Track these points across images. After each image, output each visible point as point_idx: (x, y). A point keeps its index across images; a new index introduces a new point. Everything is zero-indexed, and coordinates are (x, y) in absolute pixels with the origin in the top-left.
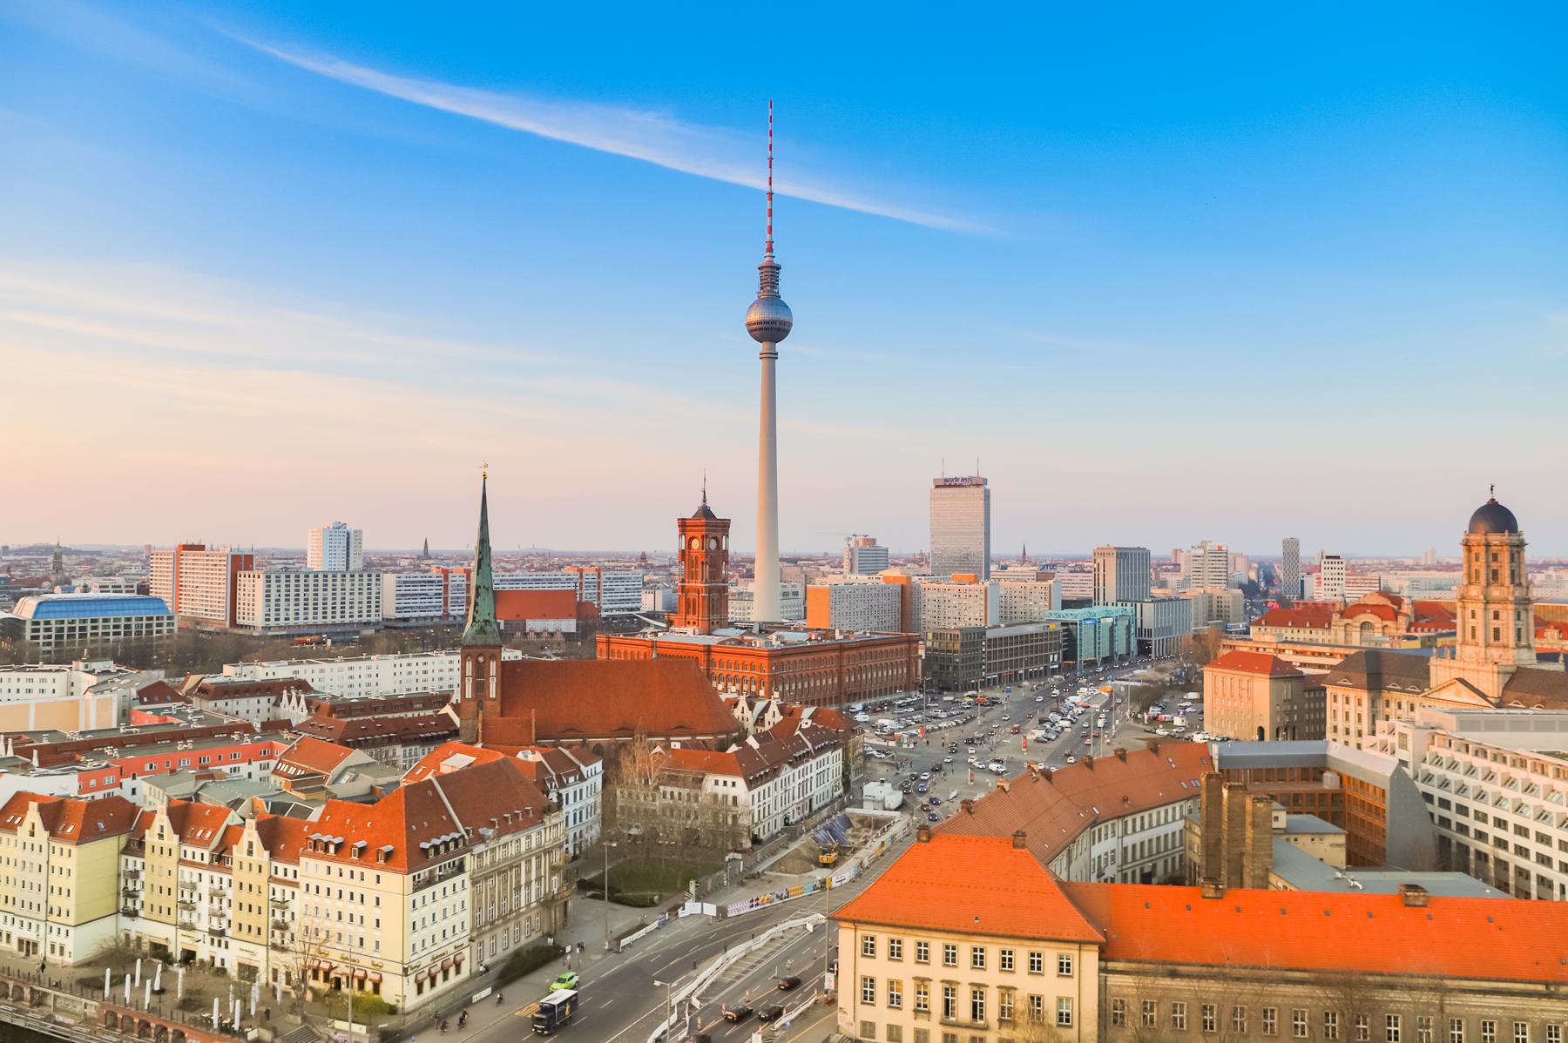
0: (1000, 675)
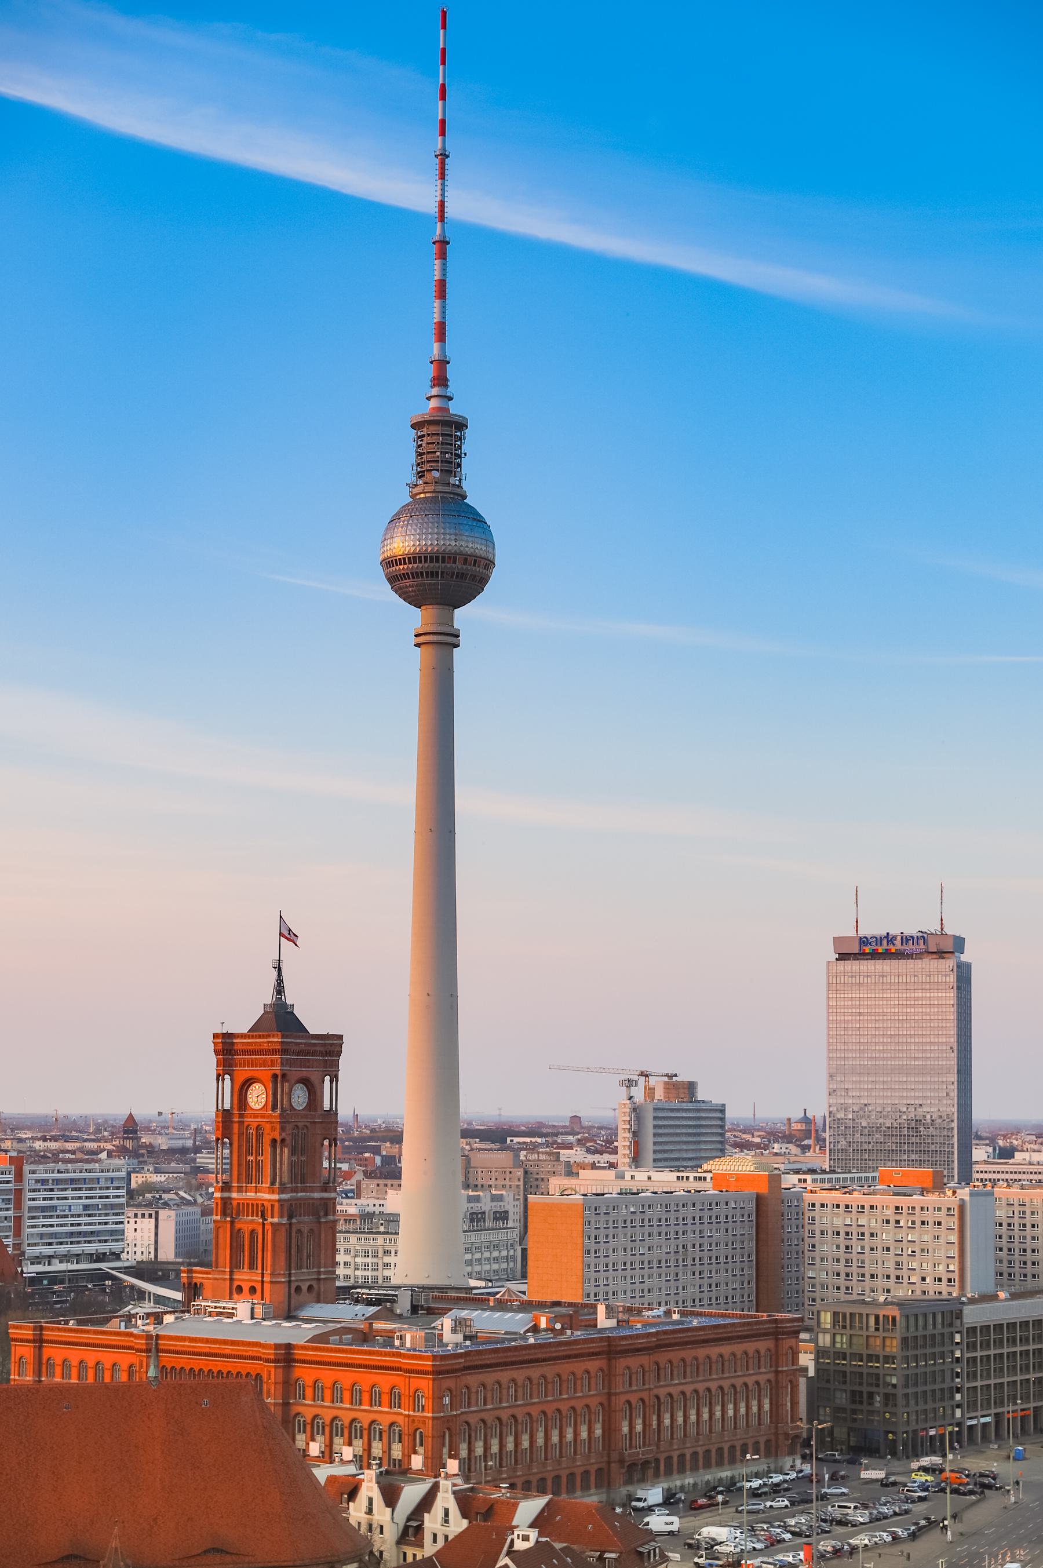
0: (997, 1415)
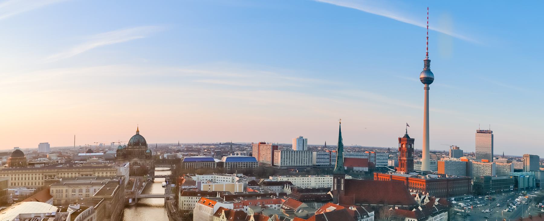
0: (495, 191)
